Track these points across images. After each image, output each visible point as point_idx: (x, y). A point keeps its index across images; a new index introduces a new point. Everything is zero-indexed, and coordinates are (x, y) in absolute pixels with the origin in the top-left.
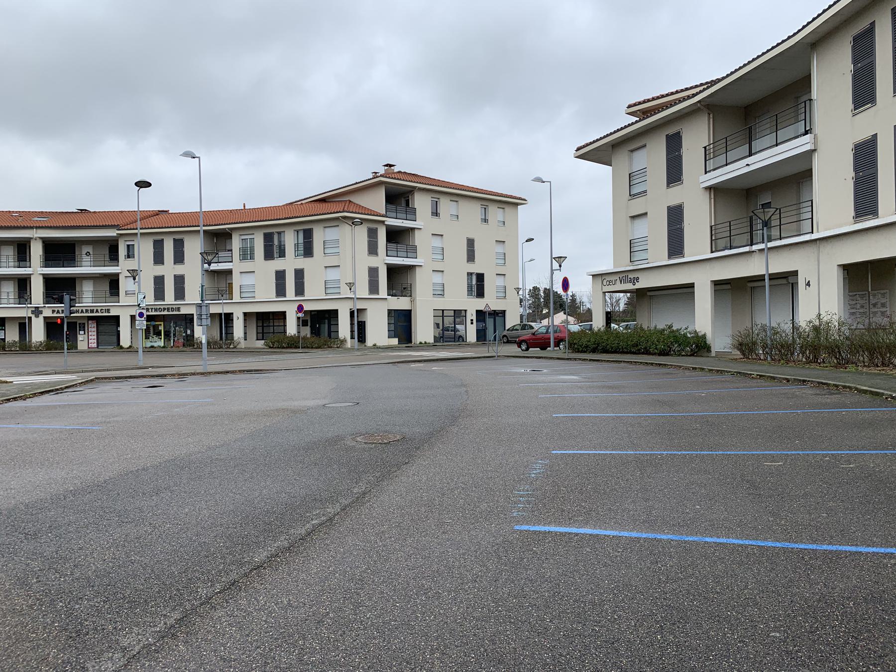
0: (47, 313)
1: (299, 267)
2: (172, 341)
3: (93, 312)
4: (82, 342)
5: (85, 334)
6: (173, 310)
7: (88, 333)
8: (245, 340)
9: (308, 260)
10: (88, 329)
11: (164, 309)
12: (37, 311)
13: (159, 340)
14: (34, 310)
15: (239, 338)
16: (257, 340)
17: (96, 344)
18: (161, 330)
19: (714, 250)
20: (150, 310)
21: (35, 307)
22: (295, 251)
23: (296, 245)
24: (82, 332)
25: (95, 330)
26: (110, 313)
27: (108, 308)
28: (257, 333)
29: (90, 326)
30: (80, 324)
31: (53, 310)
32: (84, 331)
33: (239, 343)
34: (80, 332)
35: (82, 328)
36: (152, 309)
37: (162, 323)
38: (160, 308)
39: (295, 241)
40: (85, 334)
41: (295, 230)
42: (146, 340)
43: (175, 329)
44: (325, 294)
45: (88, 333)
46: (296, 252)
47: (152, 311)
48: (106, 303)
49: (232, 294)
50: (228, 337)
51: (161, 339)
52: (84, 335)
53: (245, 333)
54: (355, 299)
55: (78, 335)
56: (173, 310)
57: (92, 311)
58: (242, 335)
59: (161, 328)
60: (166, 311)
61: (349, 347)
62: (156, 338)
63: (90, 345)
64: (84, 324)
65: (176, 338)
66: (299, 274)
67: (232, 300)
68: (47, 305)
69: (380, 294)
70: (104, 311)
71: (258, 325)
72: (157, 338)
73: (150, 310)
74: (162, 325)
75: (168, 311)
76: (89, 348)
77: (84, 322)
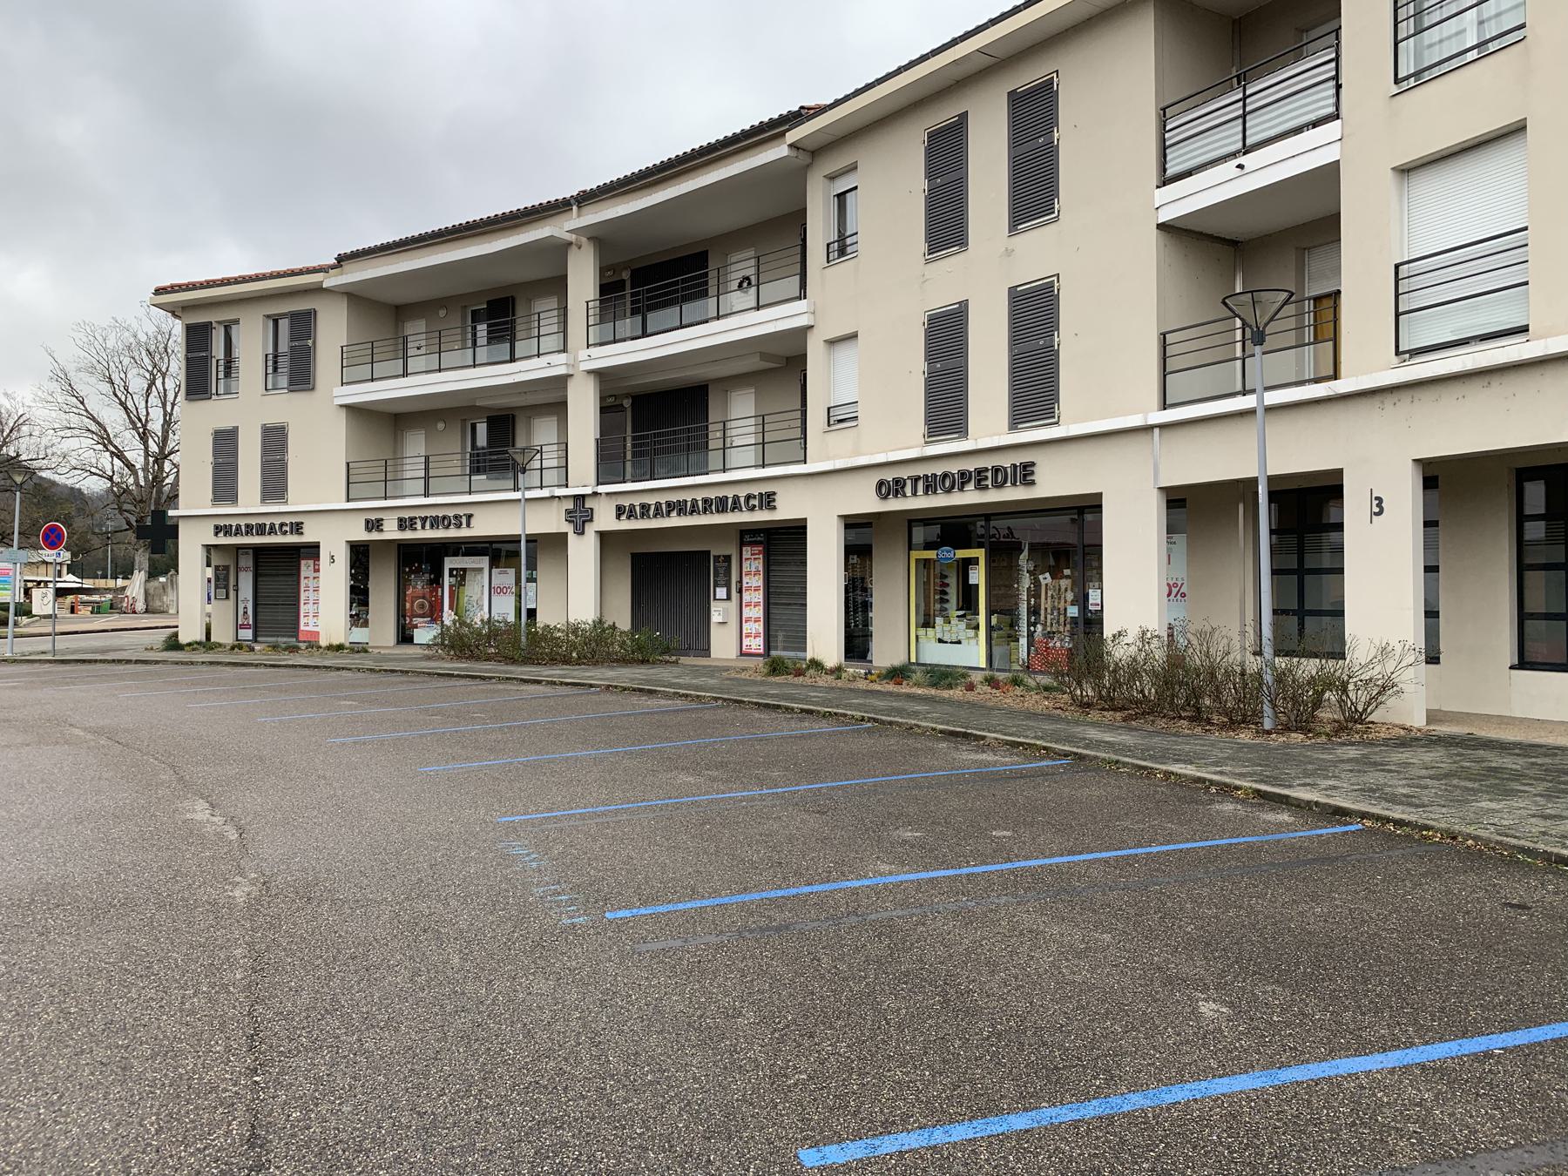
0: (605, 519)
1: (273, 419)
2: (1023, 641)
3: (263, 533)
4: (722, 629)
5: (729, 598)
6: (1000, 477)
7: (740, 591)
8: (1433, 658)
9: (300, 398)
10: (741, 582)
11: (965, 477)
12: (580, 511)
13: (971, 633)
14: (571, 506)
15: (1384, 651)
16: (1523, 663)
17: (760, 641)
18: (977, 586)
19: (270, 387)
20: (419, 526)
21: (575, 496)
22: (266, 374)
23: (270, 357)
24: (721, 592)
25: (761, 583)
26: (1033, 483)
27: (298, 520)
28: (1523, 617)
29: (746, 565)
30: (717, 558)
31: (400, 520)
32: (728, 586)
33: (1386, 687)
34: (718, 589)
35: (721, 578)
36: (424, 520)
37: (980, 553)
38: (945, 475)
39: (265, 346)
40: (729, 598)
41: (268, 317)
42: (922, 631)
43: (1037, 583)
44: (1395, 360)
45: (740, 591)
46: (270, 377)
47: (915, 494)
48: (470, 493)
49: (1336, 341)
50: (1308, 630)
51: (977, 628)
52: (728, 603)
53: (1431, 614)
54: (1259, 389)
55: (712, 603)
56: (1000, 477)
57: (261, 530)
58: (1408, 629)
59: (978, 576)
60: (971, 486)
61: (1418, 721)
62: (958, 628)
63: (746, 642)
64: (728, 559)
65: (1039, 628)
66: (275, 439)
67: (1336, 376)
68: (602, 489)
69: (1526, 323)
70: (288, 529)
71: (1528, 561)
72: (962, 625)
73: (419, 526)
74: (982, 562)
75: (980, 486)
76: (742, 654)
77: (727, 553)
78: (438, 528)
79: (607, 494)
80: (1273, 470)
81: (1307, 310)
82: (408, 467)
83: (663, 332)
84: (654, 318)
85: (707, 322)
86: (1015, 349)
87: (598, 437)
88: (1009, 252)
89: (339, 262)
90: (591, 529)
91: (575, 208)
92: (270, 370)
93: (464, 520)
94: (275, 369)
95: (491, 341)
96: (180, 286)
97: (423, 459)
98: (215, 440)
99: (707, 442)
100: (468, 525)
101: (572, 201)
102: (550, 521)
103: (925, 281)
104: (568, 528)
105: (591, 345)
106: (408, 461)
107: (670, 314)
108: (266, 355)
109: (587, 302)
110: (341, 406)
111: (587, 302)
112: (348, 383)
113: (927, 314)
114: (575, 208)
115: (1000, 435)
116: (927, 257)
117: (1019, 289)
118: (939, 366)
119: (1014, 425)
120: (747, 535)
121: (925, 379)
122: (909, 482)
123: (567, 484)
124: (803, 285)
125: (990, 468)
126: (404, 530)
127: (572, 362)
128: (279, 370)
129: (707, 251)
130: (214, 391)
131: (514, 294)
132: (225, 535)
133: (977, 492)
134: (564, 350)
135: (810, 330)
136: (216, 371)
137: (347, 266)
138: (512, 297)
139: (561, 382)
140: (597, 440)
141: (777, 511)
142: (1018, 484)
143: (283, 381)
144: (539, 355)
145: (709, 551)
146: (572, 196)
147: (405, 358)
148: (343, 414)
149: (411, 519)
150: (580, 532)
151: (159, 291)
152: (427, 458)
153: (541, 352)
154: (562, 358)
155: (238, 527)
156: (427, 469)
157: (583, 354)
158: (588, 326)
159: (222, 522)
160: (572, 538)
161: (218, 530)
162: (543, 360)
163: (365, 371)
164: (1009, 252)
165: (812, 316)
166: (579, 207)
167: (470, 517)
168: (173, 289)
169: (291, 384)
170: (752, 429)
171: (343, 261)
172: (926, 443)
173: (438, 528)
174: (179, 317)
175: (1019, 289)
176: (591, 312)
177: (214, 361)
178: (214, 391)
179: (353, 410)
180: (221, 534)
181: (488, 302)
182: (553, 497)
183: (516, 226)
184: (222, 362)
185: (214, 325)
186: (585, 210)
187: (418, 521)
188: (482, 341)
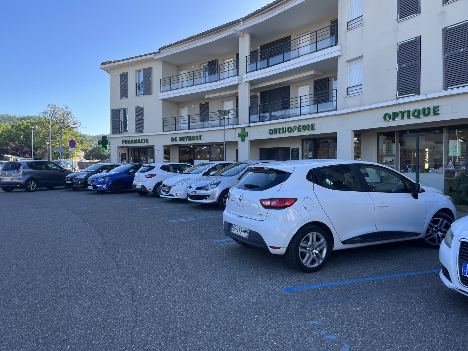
1: (139, 105)
11: (395, 115)
19: (138, 94)
22: (137, 90)
41: (137, 71)
46: (138, 91)
47: (280, 133)
66: (139, 112)
75: (299, 131)
78: (191, 140)
79: (253, 126)
80: (226, 141)
81: (332, 96)
82: (182, 120)
83: (276, 64)
84: (272, 60)
85: (290, 60)
86: (446, 54)
87: (250, 106)
88: (443, 13)
89: (159, 51)
90: (247, 139)
91: (242, 23)
92: (138, 89)
93: (199, 137)
94: (139, 88)
95: (210, 74)
96: (109, 62)
97: (187, 117)
98: (121, 77)
99: (290, 106)
100: (200, 139)
101: (241, 20)
102: (231, 136)
103: (398, 31)
104: (239, 139)
105: (248, 72)
106: (182, 118)
107: (279, 58)
108: (136, 84)
109: (246, 57)
110: (160, 99)
111: (246, 57)
112: (163, 92)
113: (398, 44)
114: (242, 23)
115: (440, 92)
116: (398, 20)
117: (448, 28)
118: (404, 65)
119: (446, 86)
120: (304, 139)
121: (397, 71)
122: (278, 130)
123: (238, 123)
124: (336, 41)
125: (407, 111)
126: (173, 141)
127: (240, 79)
128: (140, 89)
129: (290, 36)
130: (120, 131)
131: (218, 59)
132: (125, 143)
133: (298, 132)
134: (238, 75)
135: (340, 57)
136: (121, 125)
137: (162, 51)
138: (217, 59)
139: (236, 87)
140: (249, 107)
141: (439, 116)
142: (310, 130)
143: (142, 92)
144: (228, 78)
145: (290, 147)
146: (241, 18)
147: (182, 82)
148: (161, 102)
149: (183, 137)
150: (243, 140)
151: (103, 64)
152: (189, 116)
153: (229, 76)
154: (237, 78)
155: (129, 141)
156: (189, 120)
157: (245, 76)
158: (246, 65)
159: (124, 139)
160: (240, 142)
161: (123, 142)
162: (230, 79)
163: (168, 87)
164: (443, 13)
165: (340, 52)
166: (243, 22)
167: (201, 136)
168: (107, 63)
169: (144, 93)
170: (308, 100)
171: (160, 50)
172: (397, 98)
173: (191, 140)
174: (109, 73)
175: (448, 28)
176: (248, 60)
177: (120, 121)
178: (120, 131)
179: (164, 100)
180: (124, 143)
181: (209, 62)
182: (233, 128)
183: (219, 32)
184: (123, 122)
185: (120, 110)
186: (245, 23)
187: (185, 138)
188: (207, 74)
